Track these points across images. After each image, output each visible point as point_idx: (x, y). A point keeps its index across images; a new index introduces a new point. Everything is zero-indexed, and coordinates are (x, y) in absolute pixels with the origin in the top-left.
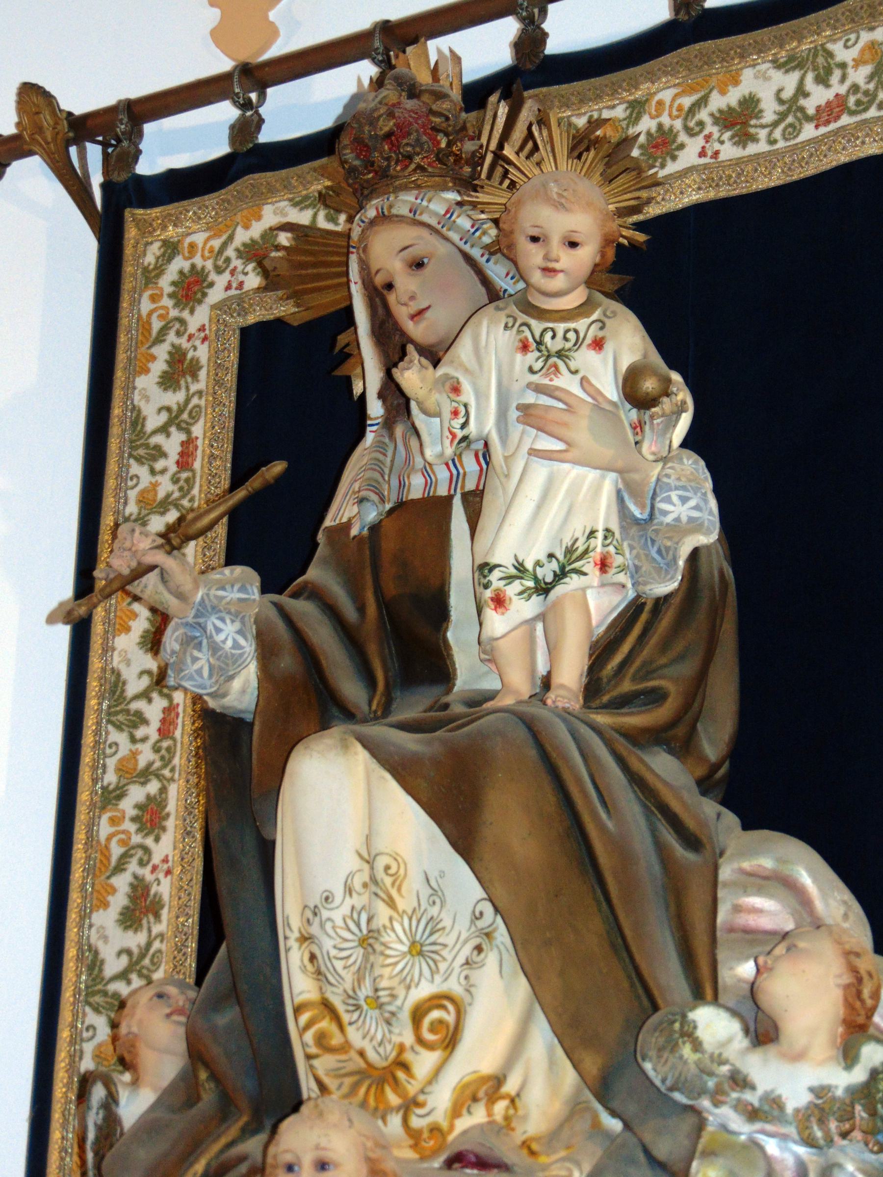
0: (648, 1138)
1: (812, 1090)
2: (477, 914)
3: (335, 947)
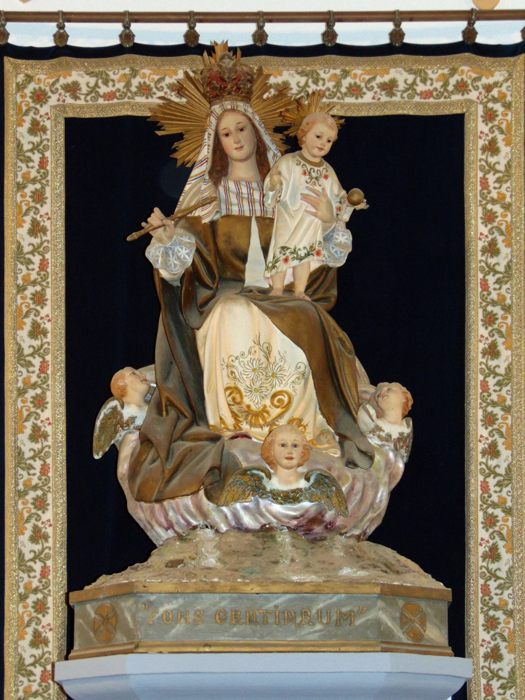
0: (357, 444)
1: (399, 433)
3: (243, 371)
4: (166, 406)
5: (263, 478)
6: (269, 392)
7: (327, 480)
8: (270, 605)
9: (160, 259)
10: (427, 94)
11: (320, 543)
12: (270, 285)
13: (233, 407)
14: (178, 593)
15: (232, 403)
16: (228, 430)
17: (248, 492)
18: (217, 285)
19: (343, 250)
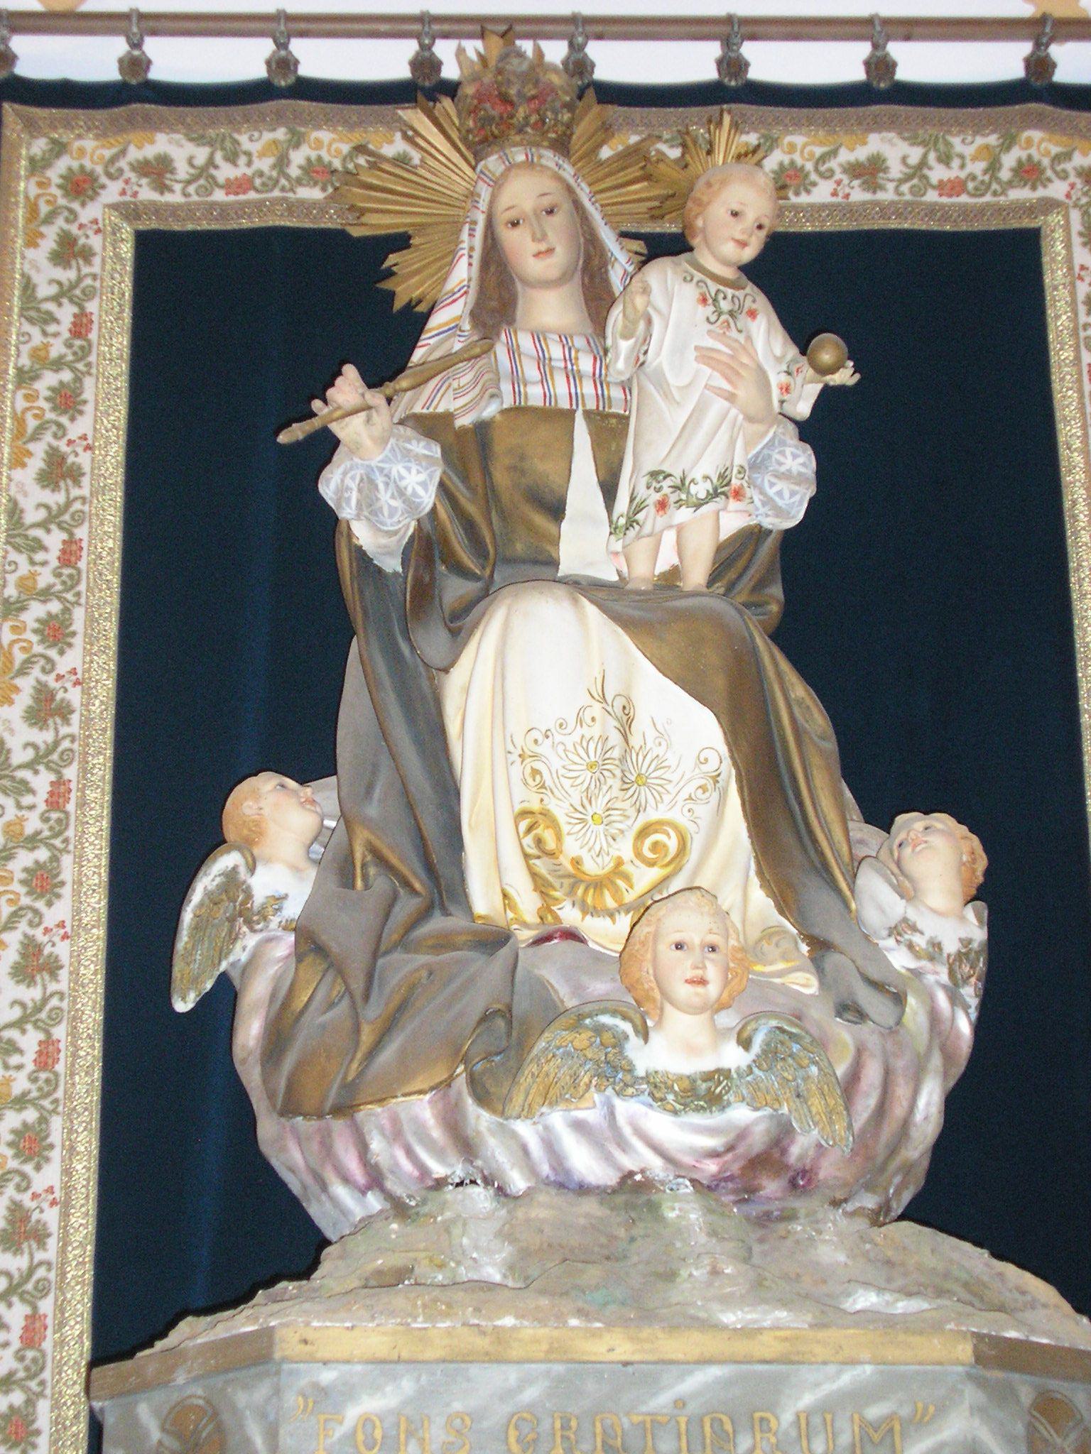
1: (961, 940)
2: (703, 761)
3: (564, 767)
4: (364, 866)
5: (627, 1037)
6: (630, 822)
7: (795, 1048)
8: (661, 1401)
9: (354, 496)
10: (956, 187)
11: (781, 1228)
12: (619, 573)
13: (537, 862)
14: (399, 1361)
15: (533, 851)
16: (525, 925)
17: (586, 1079)
18: (492, 572)
19: (797, 488)
